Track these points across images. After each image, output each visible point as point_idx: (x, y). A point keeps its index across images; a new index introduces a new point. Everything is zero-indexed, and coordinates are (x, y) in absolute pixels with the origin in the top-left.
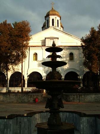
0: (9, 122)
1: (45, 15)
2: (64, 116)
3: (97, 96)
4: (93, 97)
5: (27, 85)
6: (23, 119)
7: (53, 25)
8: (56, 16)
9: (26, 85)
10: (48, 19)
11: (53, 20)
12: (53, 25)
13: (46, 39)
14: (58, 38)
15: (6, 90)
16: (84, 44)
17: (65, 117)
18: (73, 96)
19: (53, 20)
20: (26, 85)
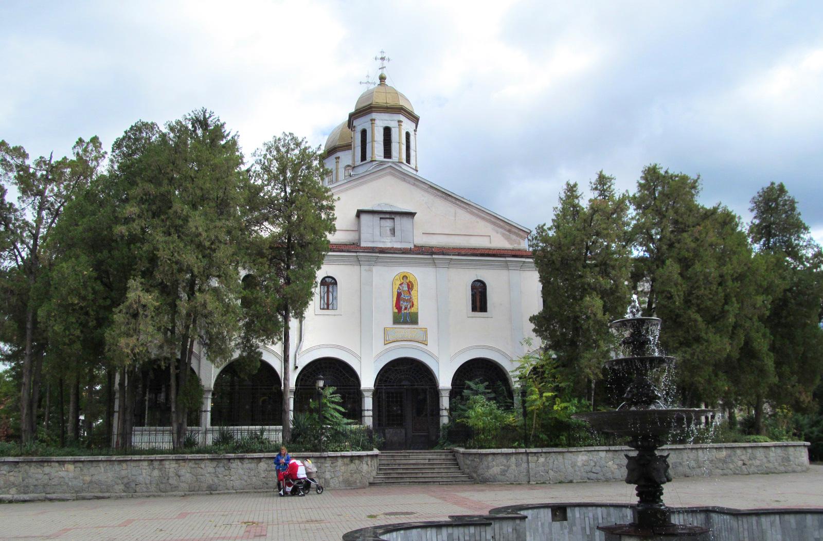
0: (483, 534)
1: (353, 110)
2: (587, 519)
3: (595, 457)
4: (579, 464)
5: (209, 414)
6: (501, 529)
7: (388, 153)
8: (402, 118)
9: (207, 418)
10: (367, 126)
11: (387, 131)
12: (388, 153)
13: (488, 238)
14: (412, 215)
15: (117, 437)
16: (68, 161)
17: (592, 522)
18: (502, 460)
19: (387, 131)
20: (207, 418)
